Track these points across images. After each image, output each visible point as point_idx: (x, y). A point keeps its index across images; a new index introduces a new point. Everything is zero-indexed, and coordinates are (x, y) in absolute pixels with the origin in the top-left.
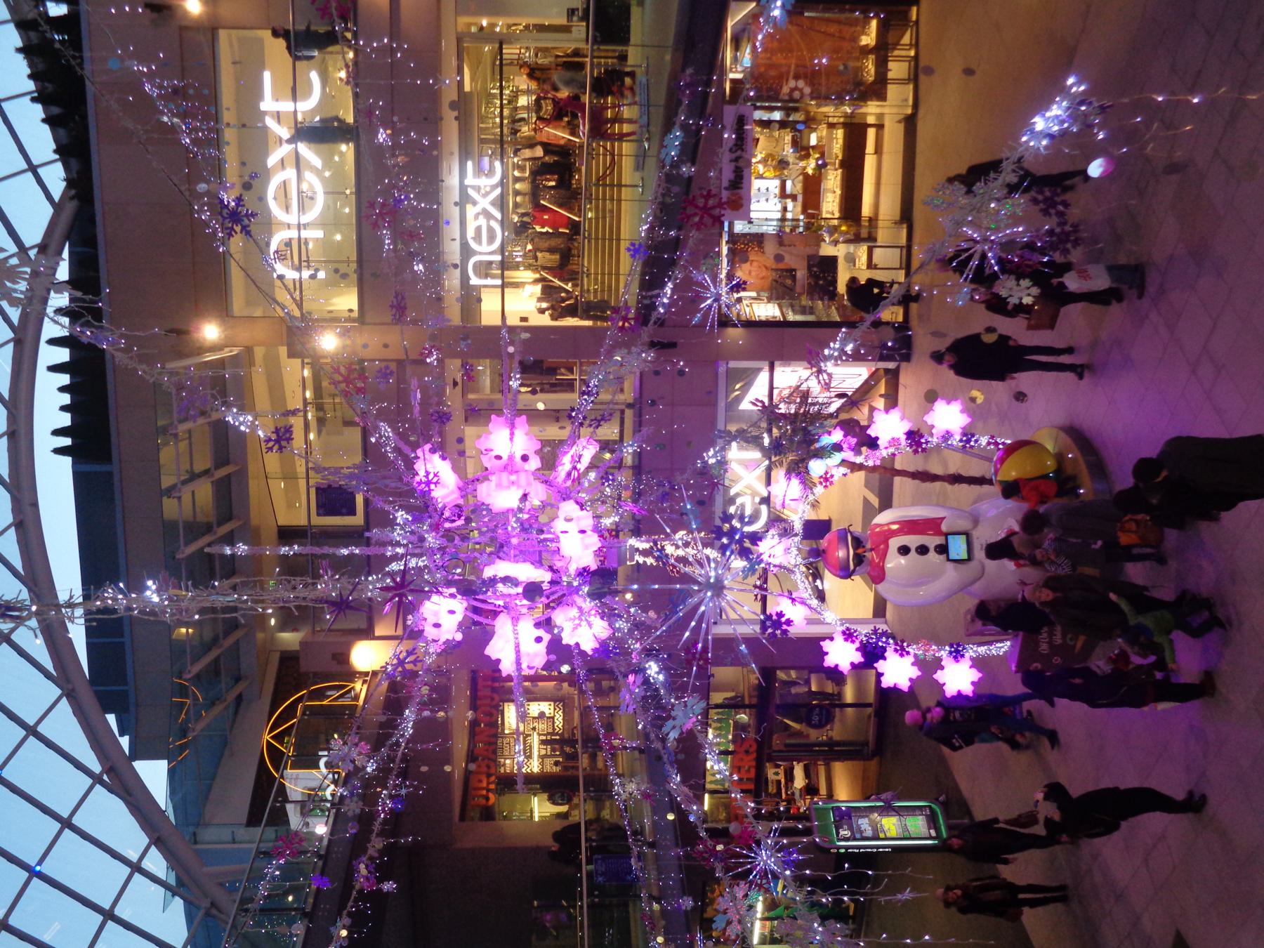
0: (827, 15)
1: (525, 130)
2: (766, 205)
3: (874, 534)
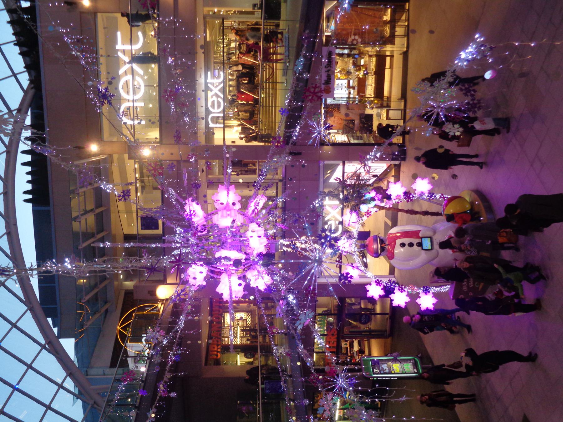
0: (368, 7)
1: (234, 58)
2: (341, 91)
3: (389, 238)
